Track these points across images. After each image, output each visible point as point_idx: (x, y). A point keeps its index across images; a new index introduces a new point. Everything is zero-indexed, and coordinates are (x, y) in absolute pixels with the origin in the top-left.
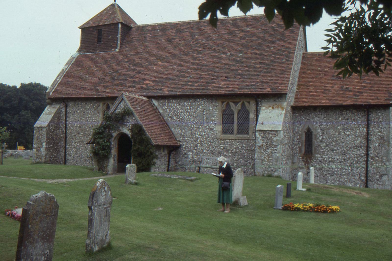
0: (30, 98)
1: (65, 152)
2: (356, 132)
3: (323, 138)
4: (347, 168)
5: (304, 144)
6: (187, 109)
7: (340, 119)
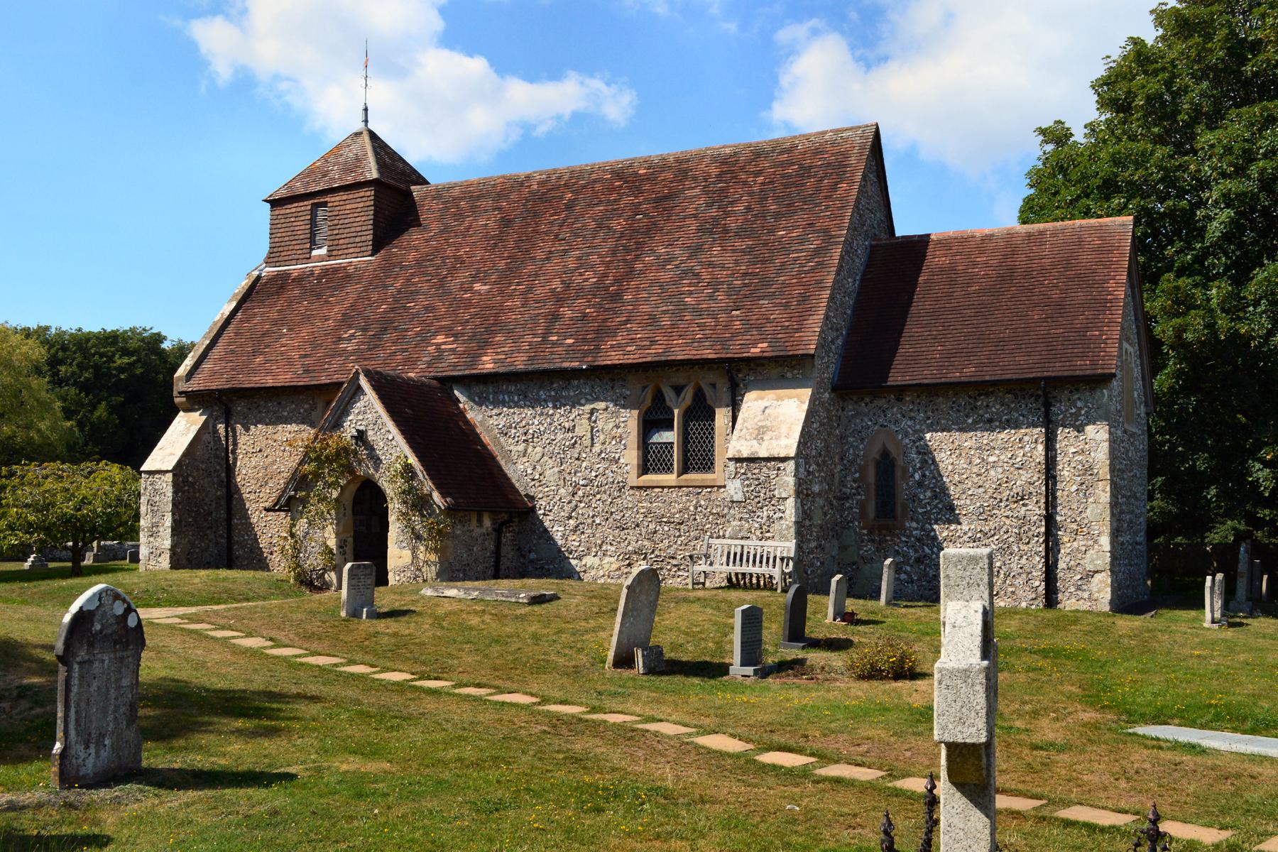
0: (116, 388)
1: (229, 538)
3: (924, 476)
5: (873, 492)
7: (970, 421)
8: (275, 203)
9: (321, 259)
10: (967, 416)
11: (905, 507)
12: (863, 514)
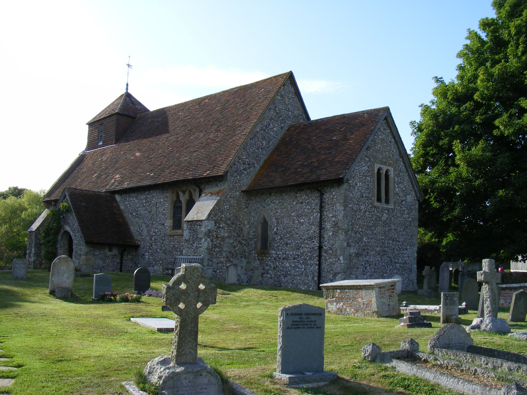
2: (310, 219)
4: (300, 266)
6: (143, 203)
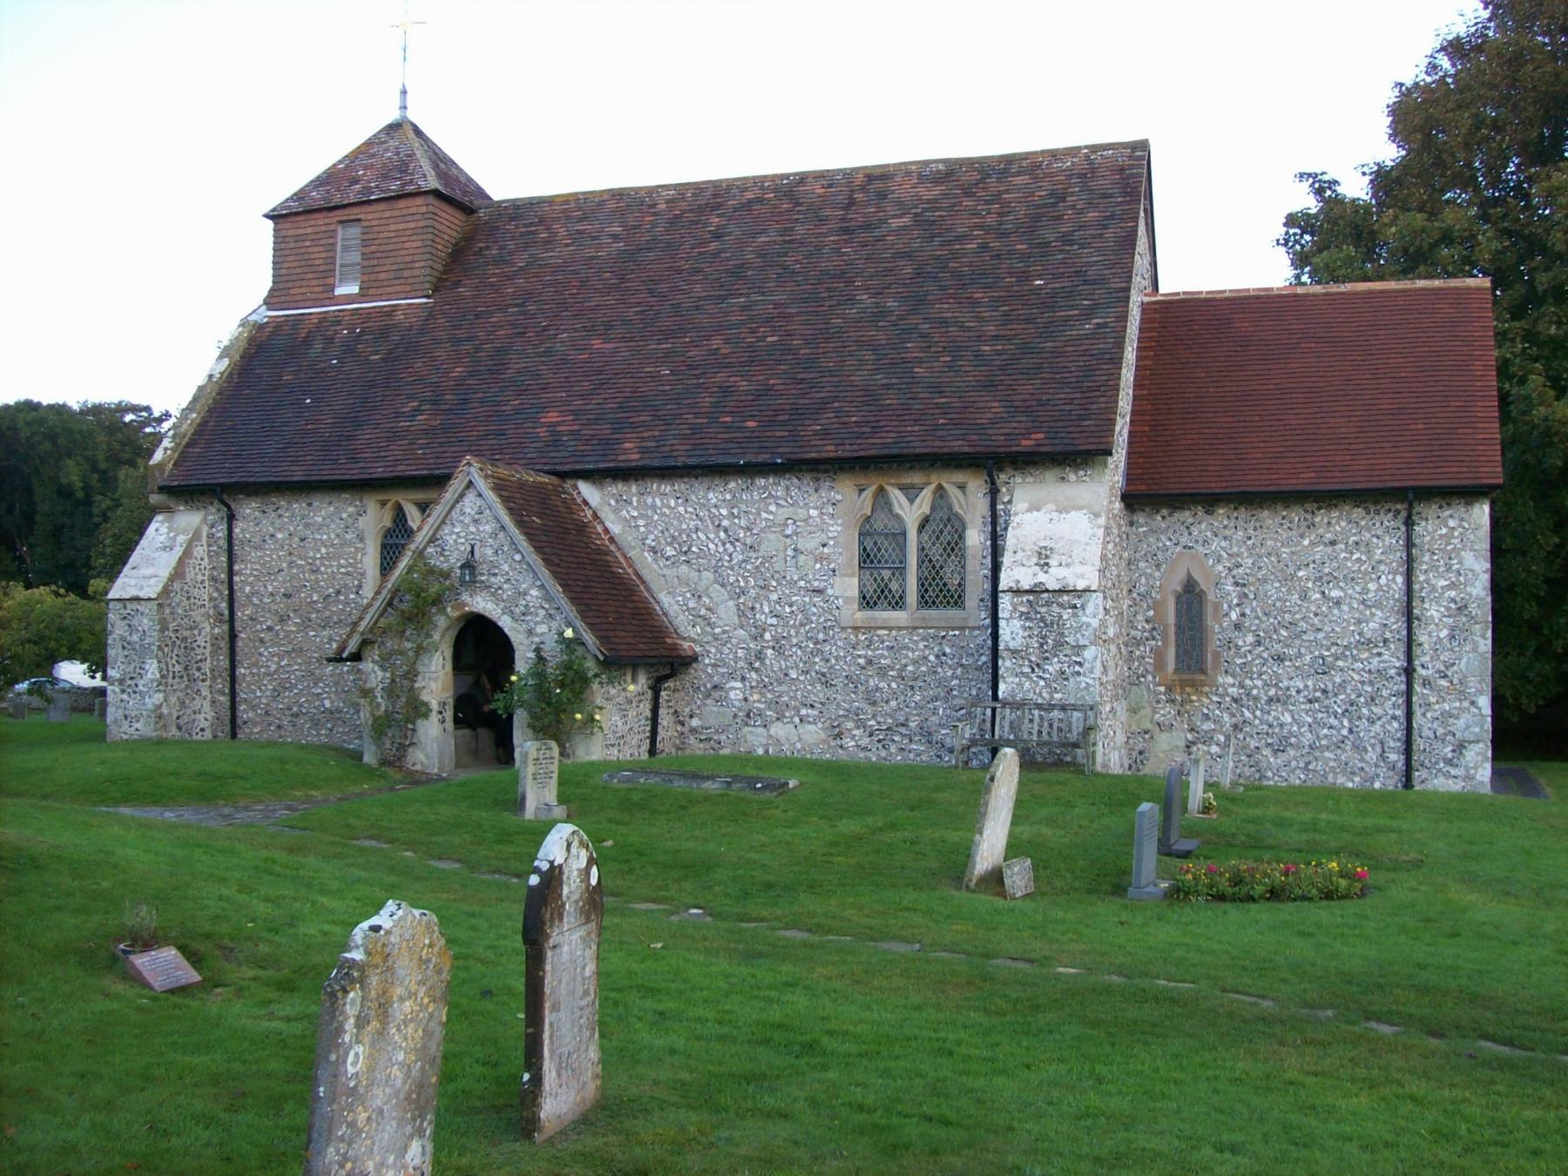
1: (233, 694)
3: (1243, 615)
5: (1172, 638)
7: (1306, 542)
8: (275, 216)
9: (349, 299)
10: (1302, 536)
11: (1217, 656)
12: (1159, 665)
